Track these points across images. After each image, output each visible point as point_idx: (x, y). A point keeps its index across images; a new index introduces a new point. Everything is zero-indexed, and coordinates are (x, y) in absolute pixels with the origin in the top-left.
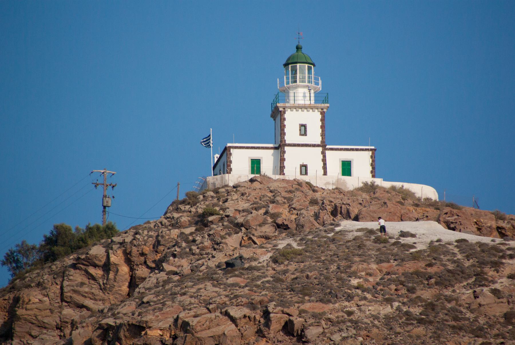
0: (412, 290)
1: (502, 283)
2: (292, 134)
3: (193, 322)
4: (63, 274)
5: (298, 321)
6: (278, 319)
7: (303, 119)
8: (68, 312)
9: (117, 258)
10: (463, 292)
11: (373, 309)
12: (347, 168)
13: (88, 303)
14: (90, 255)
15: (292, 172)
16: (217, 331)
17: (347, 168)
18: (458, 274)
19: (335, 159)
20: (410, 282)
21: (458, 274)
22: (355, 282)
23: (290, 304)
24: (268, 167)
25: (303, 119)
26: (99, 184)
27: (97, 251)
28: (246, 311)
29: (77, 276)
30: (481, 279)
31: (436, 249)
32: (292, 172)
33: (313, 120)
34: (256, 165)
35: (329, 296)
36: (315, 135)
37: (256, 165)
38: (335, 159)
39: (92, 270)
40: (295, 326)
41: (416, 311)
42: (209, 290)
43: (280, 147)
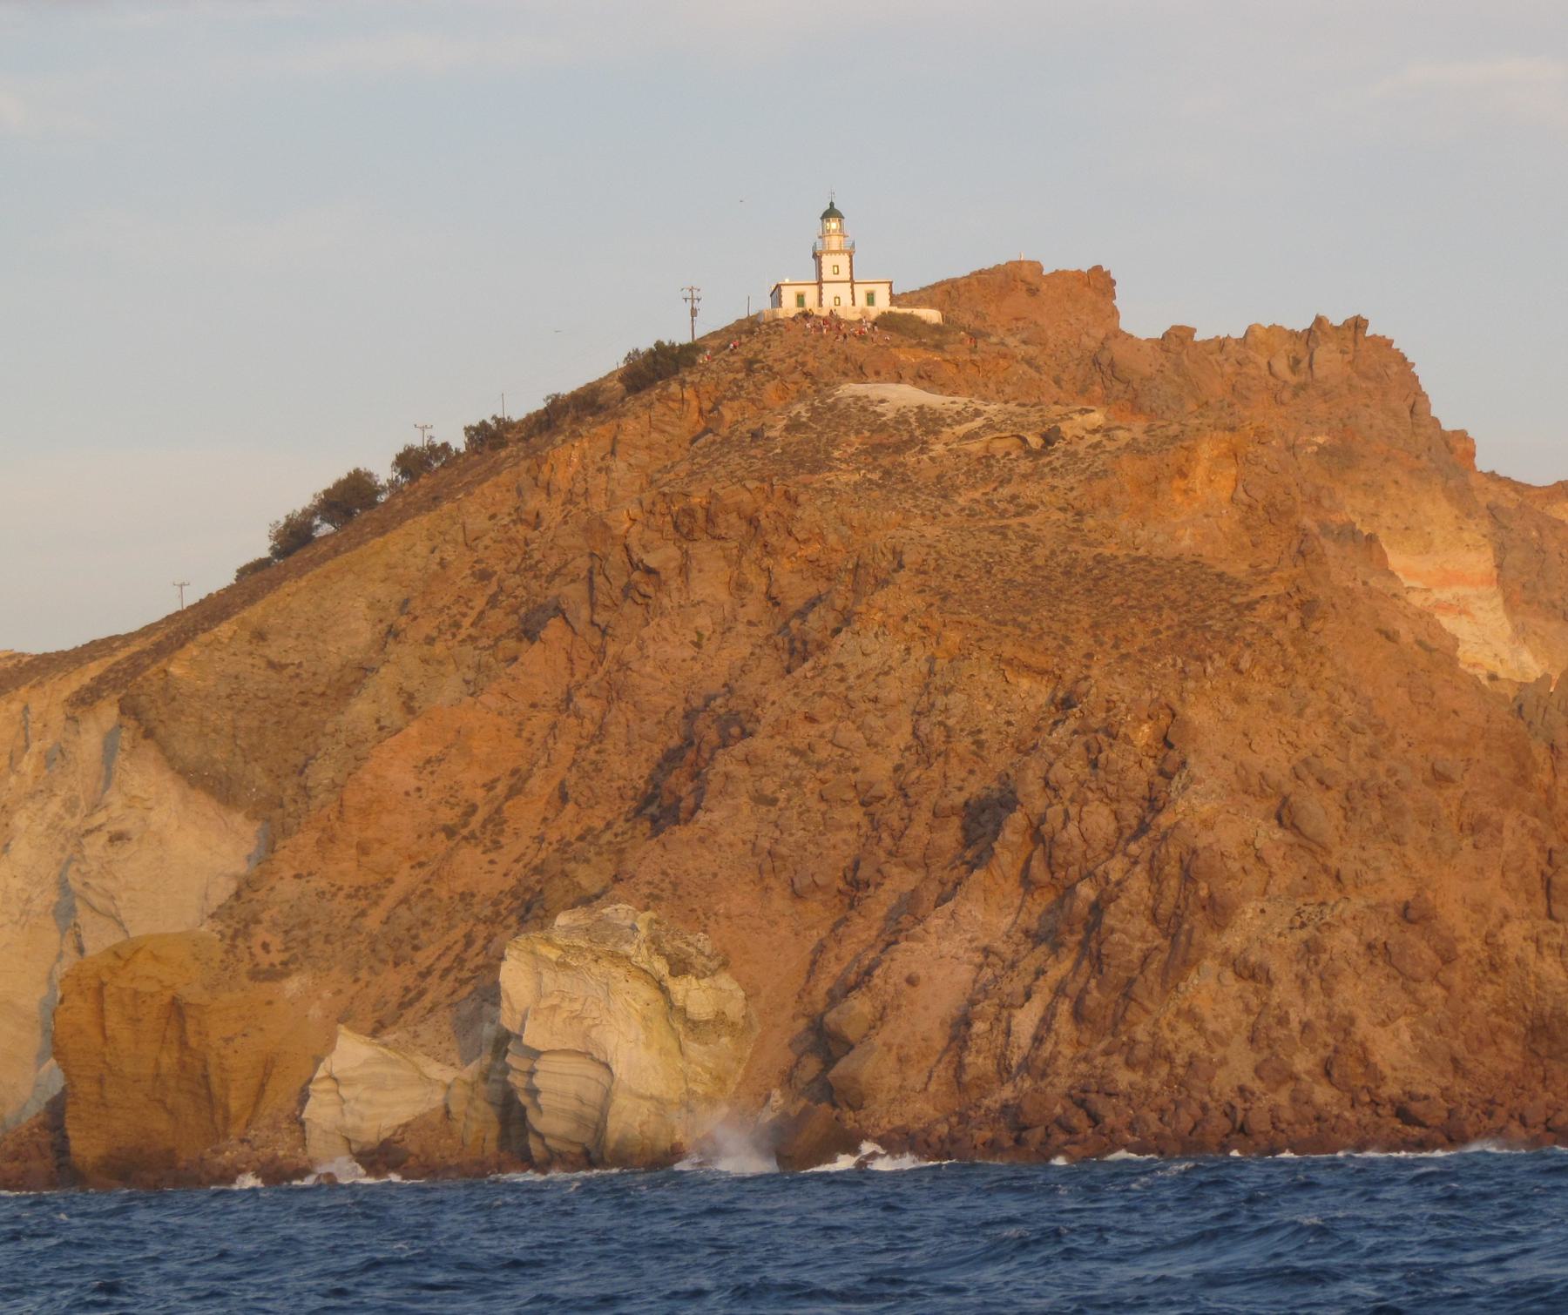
0: (875, 459)
3: (721, 493)
4: (650, 406)
5: (793, 490)
8: (655, 435)
10: (910, 458)
11: (844, 478)
12: (870, 299)
13: (668, 428)
15: (828, 301)
16: (738, 499)
17: (870, 299)
20: (878, 448)
22: (836, 454)
23: (789, 477)
28: (757, 484)
29: (659, 408)
34: (800, 299)
37: (800, 299)
38: (861, 292)
39: (671, 404)
40: (334, 1057)
41: (875, 476)
43: (820, 283)
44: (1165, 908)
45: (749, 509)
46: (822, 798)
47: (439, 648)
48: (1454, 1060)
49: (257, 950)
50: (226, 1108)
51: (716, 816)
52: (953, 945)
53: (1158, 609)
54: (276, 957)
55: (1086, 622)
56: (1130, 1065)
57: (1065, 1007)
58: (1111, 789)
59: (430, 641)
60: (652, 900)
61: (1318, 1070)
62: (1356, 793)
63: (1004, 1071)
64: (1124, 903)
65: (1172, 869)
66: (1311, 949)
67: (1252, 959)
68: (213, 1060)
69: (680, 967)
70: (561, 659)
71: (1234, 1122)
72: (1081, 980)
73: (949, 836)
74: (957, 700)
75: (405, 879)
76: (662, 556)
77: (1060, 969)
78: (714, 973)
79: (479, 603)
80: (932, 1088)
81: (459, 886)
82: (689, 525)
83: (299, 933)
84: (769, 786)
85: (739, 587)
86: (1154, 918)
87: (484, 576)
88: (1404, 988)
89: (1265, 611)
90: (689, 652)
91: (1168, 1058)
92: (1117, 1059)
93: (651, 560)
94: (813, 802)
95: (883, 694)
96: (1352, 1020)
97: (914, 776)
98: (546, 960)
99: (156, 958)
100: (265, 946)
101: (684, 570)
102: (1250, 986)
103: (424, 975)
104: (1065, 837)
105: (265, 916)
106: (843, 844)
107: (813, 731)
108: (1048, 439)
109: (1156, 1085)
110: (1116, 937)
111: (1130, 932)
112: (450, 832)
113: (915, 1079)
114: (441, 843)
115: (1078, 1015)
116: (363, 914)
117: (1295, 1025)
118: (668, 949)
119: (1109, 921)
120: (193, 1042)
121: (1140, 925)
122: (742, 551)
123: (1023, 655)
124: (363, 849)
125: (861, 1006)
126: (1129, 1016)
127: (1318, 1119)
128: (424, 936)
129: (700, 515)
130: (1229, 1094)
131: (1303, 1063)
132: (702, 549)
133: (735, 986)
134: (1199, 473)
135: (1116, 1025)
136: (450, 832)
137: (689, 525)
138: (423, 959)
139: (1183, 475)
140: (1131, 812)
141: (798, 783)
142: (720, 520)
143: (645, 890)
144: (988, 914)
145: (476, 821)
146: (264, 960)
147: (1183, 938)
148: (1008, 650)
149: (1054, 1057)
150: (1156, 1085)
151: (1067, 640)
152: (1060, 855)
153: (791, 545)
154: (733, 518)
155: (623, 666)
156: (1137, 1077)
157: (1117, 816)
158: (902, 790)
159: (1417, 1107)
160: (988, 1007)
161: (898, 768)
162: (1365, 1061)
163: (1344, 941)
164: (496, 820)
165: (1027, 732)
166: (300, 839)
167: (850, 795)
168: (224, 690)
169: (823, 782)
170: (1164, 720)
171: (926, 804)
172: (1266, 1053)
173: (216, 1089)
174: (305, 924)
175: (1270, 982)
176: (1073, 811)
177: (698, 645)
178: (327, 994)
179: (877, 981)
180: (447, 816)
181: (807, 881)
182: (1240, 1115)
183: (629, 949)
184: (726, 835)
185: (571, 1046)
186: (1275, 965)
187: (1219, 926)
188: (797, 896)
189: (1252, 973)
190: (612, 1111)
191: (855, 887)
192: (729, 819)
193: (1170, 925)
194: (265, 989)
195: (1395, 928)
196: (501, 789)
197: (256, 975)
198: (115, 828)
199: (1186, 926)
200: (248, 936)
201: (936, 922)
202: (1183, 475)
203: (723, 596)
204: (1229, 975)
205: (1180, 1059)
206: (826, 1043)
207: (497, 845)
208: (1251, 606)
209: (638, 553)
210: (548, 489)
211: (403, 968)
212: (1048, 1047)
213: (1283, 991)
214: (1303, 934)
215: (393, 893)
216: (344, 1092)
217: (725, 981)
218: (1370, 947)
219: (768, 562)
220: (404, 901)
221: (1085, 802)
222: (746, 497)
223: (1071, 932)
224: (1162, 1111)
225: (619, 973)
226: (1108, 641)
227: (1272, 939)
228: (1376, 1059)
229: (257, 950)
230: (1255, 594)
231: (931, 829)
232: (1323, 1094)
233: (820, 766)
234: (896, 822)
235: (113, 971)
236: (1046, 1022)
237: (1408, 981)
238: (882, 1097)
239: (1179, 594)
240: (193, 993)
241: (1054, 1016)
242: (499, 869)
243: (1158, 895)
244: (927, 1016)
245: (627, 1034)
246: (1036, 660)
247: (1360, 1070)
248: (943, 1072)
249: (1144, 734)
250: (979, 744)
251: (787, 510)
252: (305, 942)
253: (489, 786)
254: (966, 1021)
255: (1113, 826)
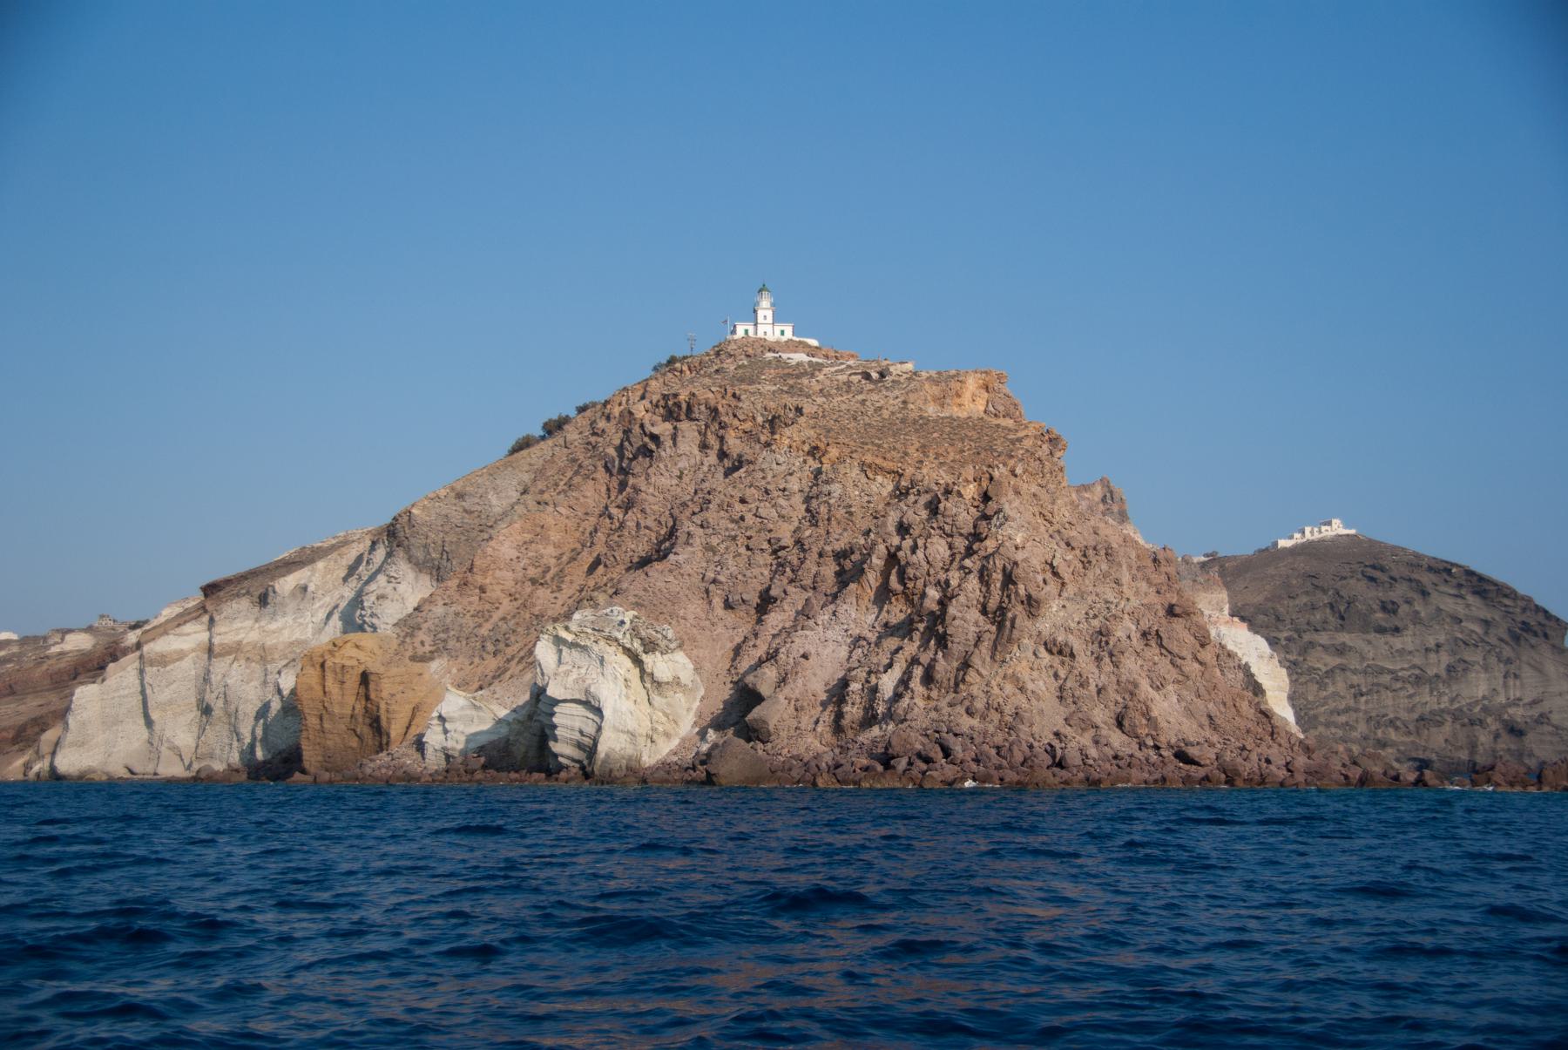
1: (821, 377)
2: (760, 319)
6: (730, 391)
7: (765, 312)
9: (685, 368)
10: (805, 381)
12: (782, 333)
14: (238, 595)
17: (782, 333)
18: (805, 373)
19: (778, 329)
20: (785, 377)
21: (805, 373)
24: (751, 333)
25: (765, 312)
26: (543, 438)
27: (678, 365)
30: (813, 375)
31: (799, 364)
32: (760, 334)
33: (769, 314)
35: (752, 382)
36: (770, 320)
42: (707, 381)
44: (993, 604)
45: (712, 403)
46: (748, 548)
47: (546, 496)
48: (1210, 717)
49: (417, 644)
50: (388, 735)
51: (680, 558)
52: (835, 633)
53: (962, 440)
54: (427, 648)
55: (917, 445)
56: (970, 712)
57: (918, 672)
58: (947, 528)
59: (542, 492)
60: (638, 605)
61: (1113, 721)
62: (1091, 552)
63: (869, 720)
64: (962, 599)
65: (998, 577)
66: (1102, 636)
67: (1060, 639)
68: (383, 706)
69: (650, 646)
70: (604, 489)
71: (1054, 757)
72: (931, 654)
73: (829, 569)
74: (836, 489)
75: (507, 606)
76: (663, 429)
77: (911, 648)
78: (673, 651)
79: (569, 474)
80: (819, 729)
81: (536, 611)
82: (672, 411)
83: (442, 636)
84: (714, 541)
85: (704, 446)
86: (984, 612)
87: (574, 460)
88: (1172, 663)
89: (1028, 443)
90: (675, 482)
91: (998, 709)
92: (961, 709)
93: (655, 430)
94: (743, 550)
95: (789, 486)
96: (1136, 685)
97: (807, 533)
98: (564, 642)
99: (357, 647)
100: (422, 643)
101: (674, 438)
102: (1057, 660)
103: (508, 661)
104: (914, 559)
105: (425, 626)
106: (761, 572)
107: (743, 508)
108: (882, 375)
109: (991, 729)
110: (957, 622)
111: (966, 620)
112: (534, 581)
113: (806, 721)
114: (528, 588)
115: (928, 679)
116: (480, 626)
117: (1093, 688)
118: (643, 634)
119: (952, 610)
120: (373, 696)
121: (974, 614)
122: (707, 426)
123: (879, 461)
124: (483, 590)
125: (770, 673)
126: (968, 678)
127: (1116, 757)
128: (513, 639)
129: (684, 406)
130: (1048, 737)
131: (1101, 715)
132: (684, 425)
133: (687, 661)
134: (967, 396)
135: (957, 685)
136: (534, 581)
137: (672, 411)
138: (510, 651)
139: (959, 396)
140: (960, 543)
141: (734, 538)
142: (696, 409)
143: (633, 600)
144: (858, 613)
145: (548, 576)
146: (421, 651)
147: (1008, 624)
148: (869, 458)
149: (910, 708)
150: (991, 729)
151: (906, 454)
152: (910, 572)
153: (736, 422)
154: (703, 408)
155: (637, 490)
156: (975, 722)
157: (951, 547)
158: (799, 542)
159: (1193, 752)
160: (861, 674)
161: (797, 530)
162: (1147, 714)
163: (1124, 630)
164: (561, 575)
165: (881, 507)
166: (449, 583)
167: (765, 546)
168: (440, 522)
169: (749, 538)
170: (985, 484)
171: (815, 550)
172: (1073, 708)
173: (384, 723)
174: (447, 630)
175: (1072, 655)
176: (920, 542)
177: (680, 477)
178: (454, 671)
179: (782, 656)
180: (532, 572)
181: (737, 597)
182: (1059, 753)
183: (620, 636)
184: (687, 569)
185: (577, 696)
186: (1077, 645)
187: (1032, 615)
188: (728, 606)
189: (1062, 651)
190: (601, 740)
191: (766, 602)
192: (689, 558)
193: (998, 617)
194: (417, 667)
195: (1164, 621)
196: (565, 558)
197: (413, 658)
198: (380, 592)
199: (1010, 615)
200: (412, 636)
201: (824, 617)
202: (959, 396)
203: (696, 451)
204: (1043, 652)
205: (1009, 709)
206: (747, 697)
207: (560, 589)
208: (1020, 440)
209: (649, 428)
210: (608, 418)
211: (499, 657)
212: (905, 702)
213: (1084, 662)
214: (1096, 623)
215: (496, 616)
216: (447, 725)
217: (680, 657)
218: (1144, 634)
219: (722, 432)
220: (504, 619)
221: (930, 536)
222: (711, 395)
223: (921, 621)
224: (998, 748)
225: (611, 650)
226: (932, 456)
227: (1073, 625)
228: (1155, 713)
229: (417, 644)
230: (1020, 434)
231: (819, 564)
232: (1117, 739)
233: (747, 529)
234: (796, 562)
235: (331, 652)
236: (904, 682)
237: (1175, 659)
238: (783, 734)
239: (974, 434)
240: (374, 666)
241: (910, 678)
242: (560, 602)
243: (987, 595)
244: (816, 680)
245: (636, 704)
246: (887, 465)
247: (1144, 721)
248: (828, 717)
249: (970, 491)
250: (851, 514)
251: (734, 402)
252: (445, 641)
253: (558, 558)
254: (844, 683)
255: (948, 552)
